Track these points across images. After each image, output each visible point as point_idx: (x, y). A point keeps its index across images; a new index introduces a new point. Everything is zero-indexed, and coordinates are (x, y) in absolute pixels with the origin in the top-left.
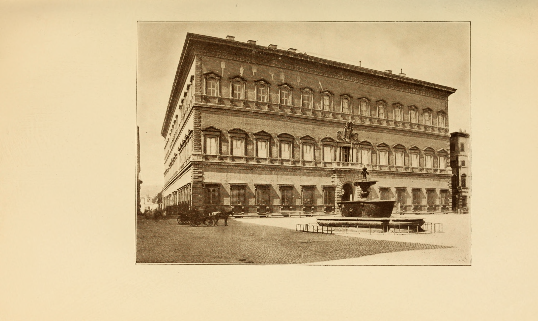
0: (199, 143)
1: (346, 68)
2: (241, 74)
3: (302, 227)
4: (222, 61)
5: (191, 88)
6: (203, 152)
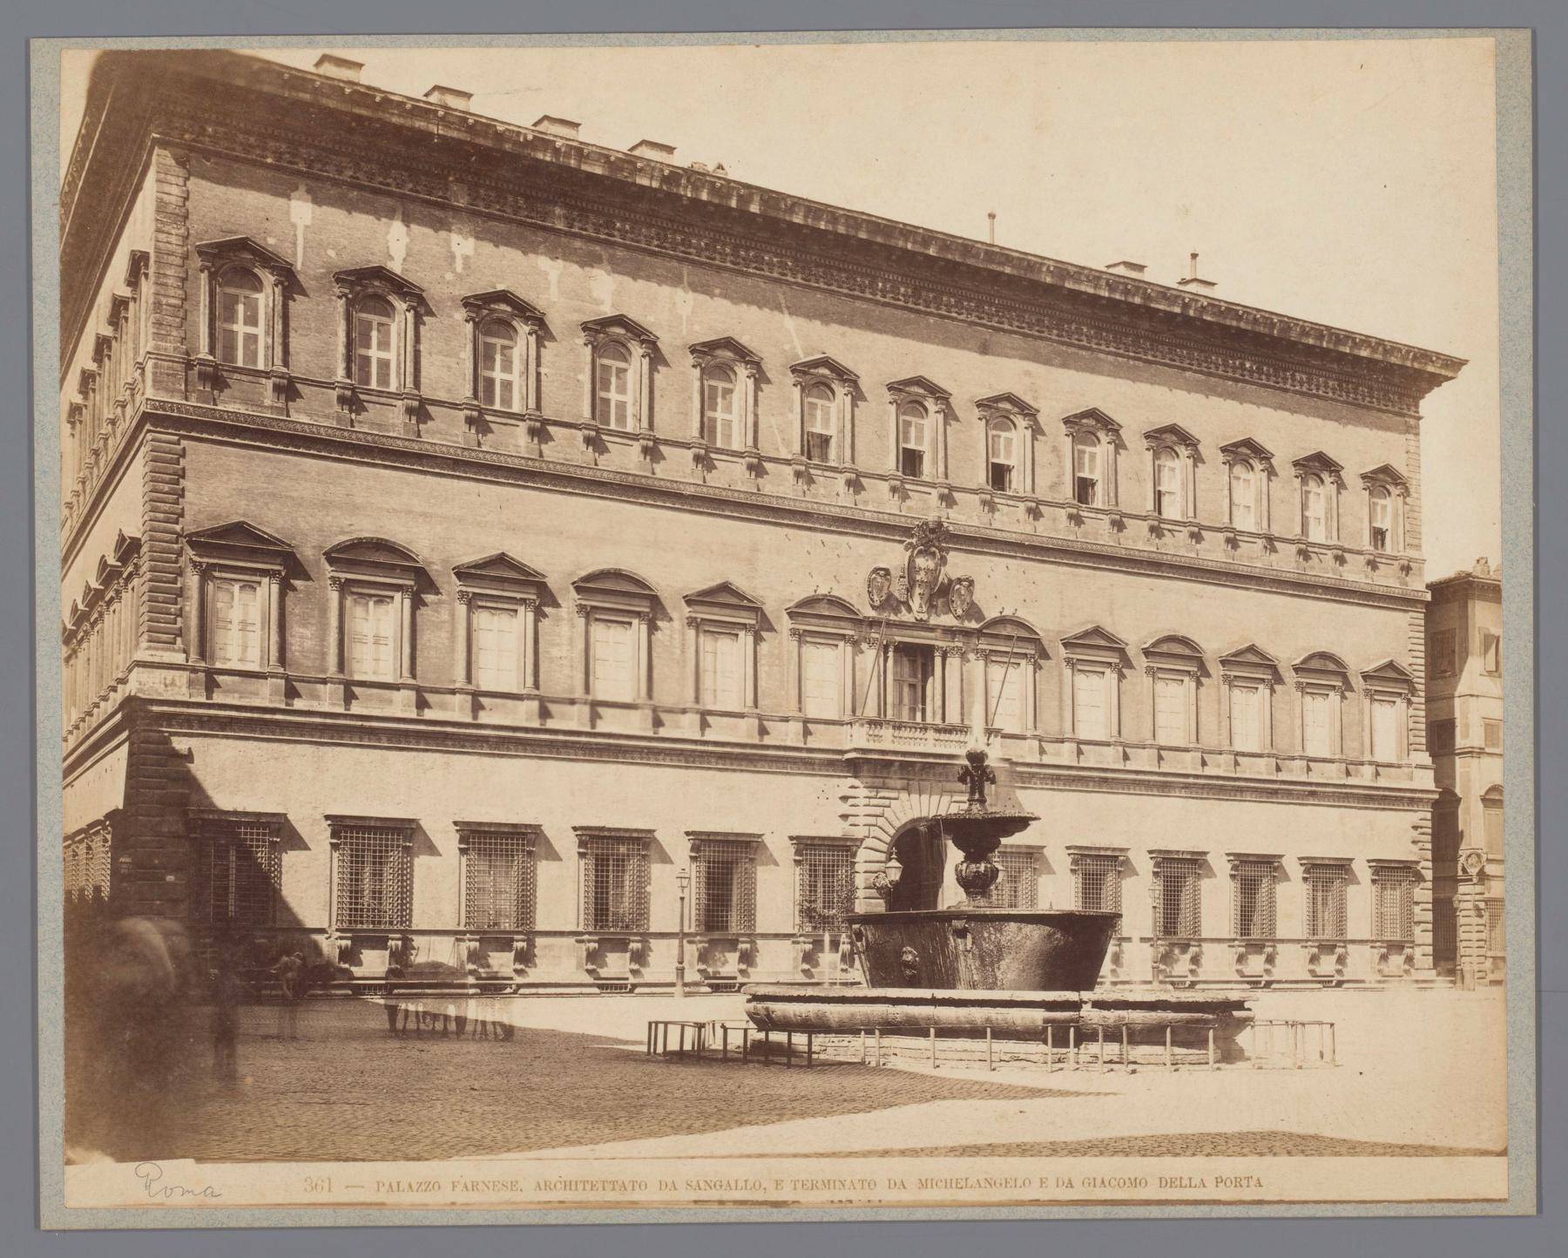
0: (173, 608)
1: (918, 248)
2: (391, 258)
3: (674, 1033)
4: (297, 189)
5: (131, 314)
6: (193, 656)
